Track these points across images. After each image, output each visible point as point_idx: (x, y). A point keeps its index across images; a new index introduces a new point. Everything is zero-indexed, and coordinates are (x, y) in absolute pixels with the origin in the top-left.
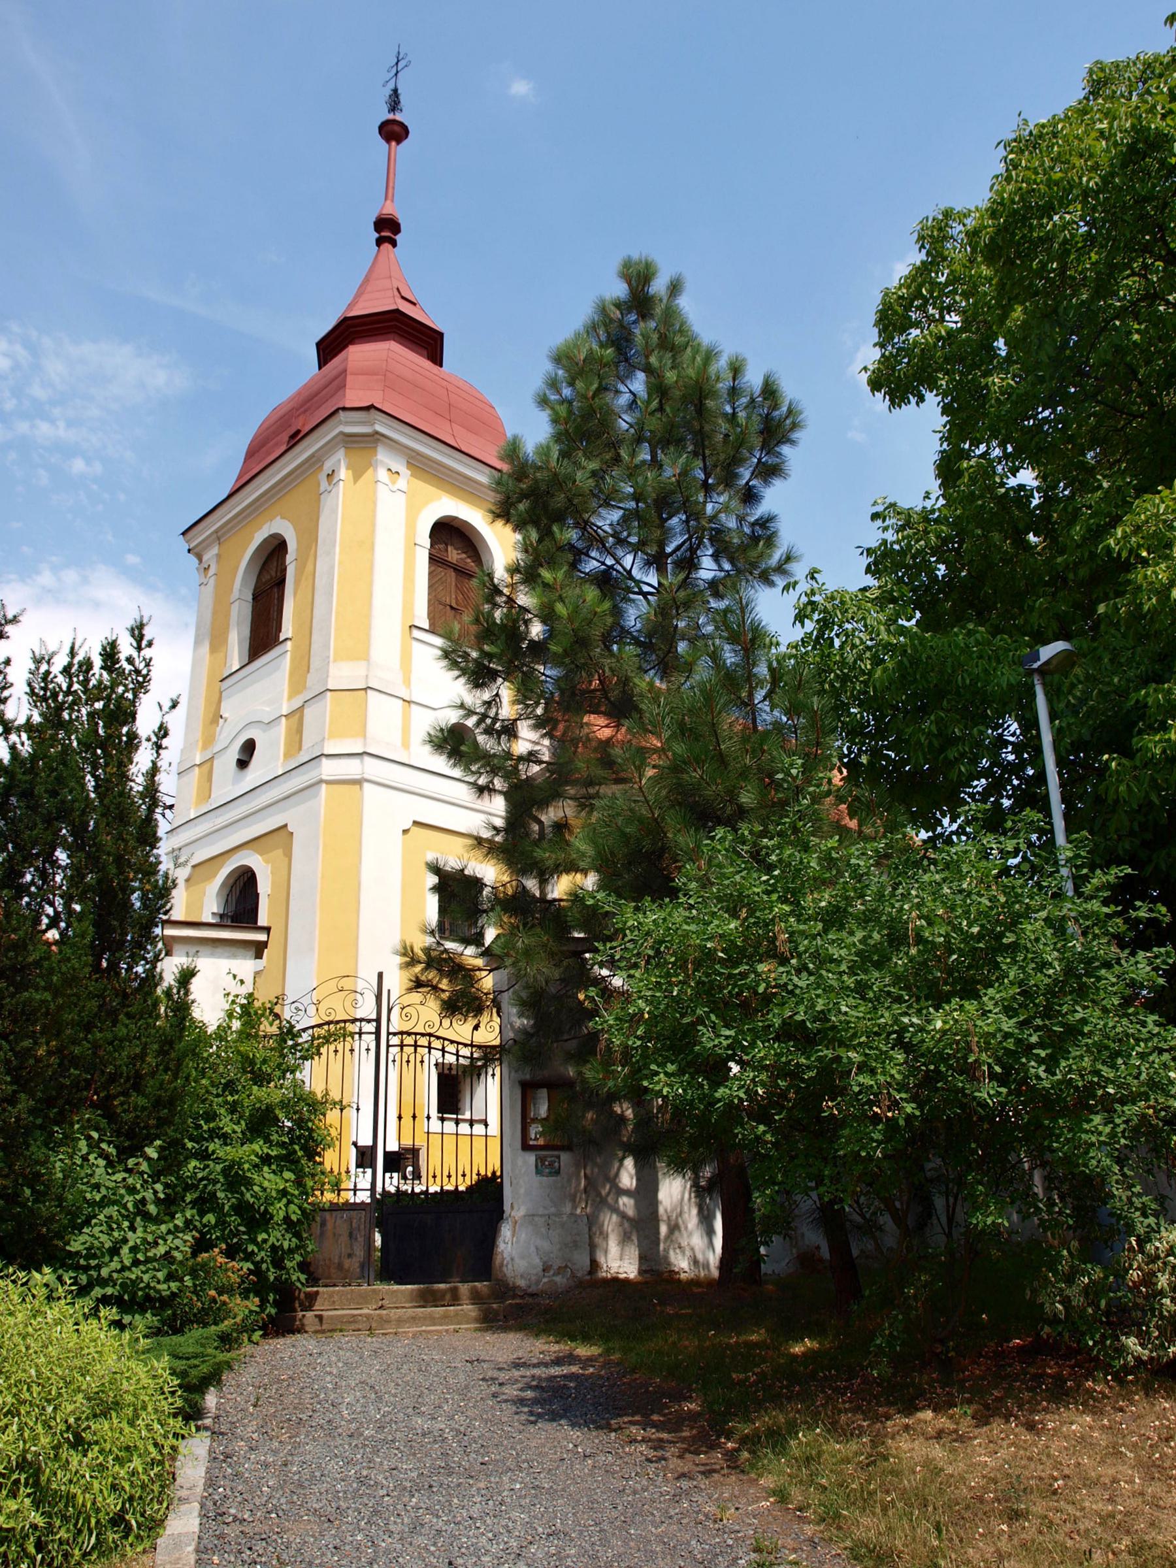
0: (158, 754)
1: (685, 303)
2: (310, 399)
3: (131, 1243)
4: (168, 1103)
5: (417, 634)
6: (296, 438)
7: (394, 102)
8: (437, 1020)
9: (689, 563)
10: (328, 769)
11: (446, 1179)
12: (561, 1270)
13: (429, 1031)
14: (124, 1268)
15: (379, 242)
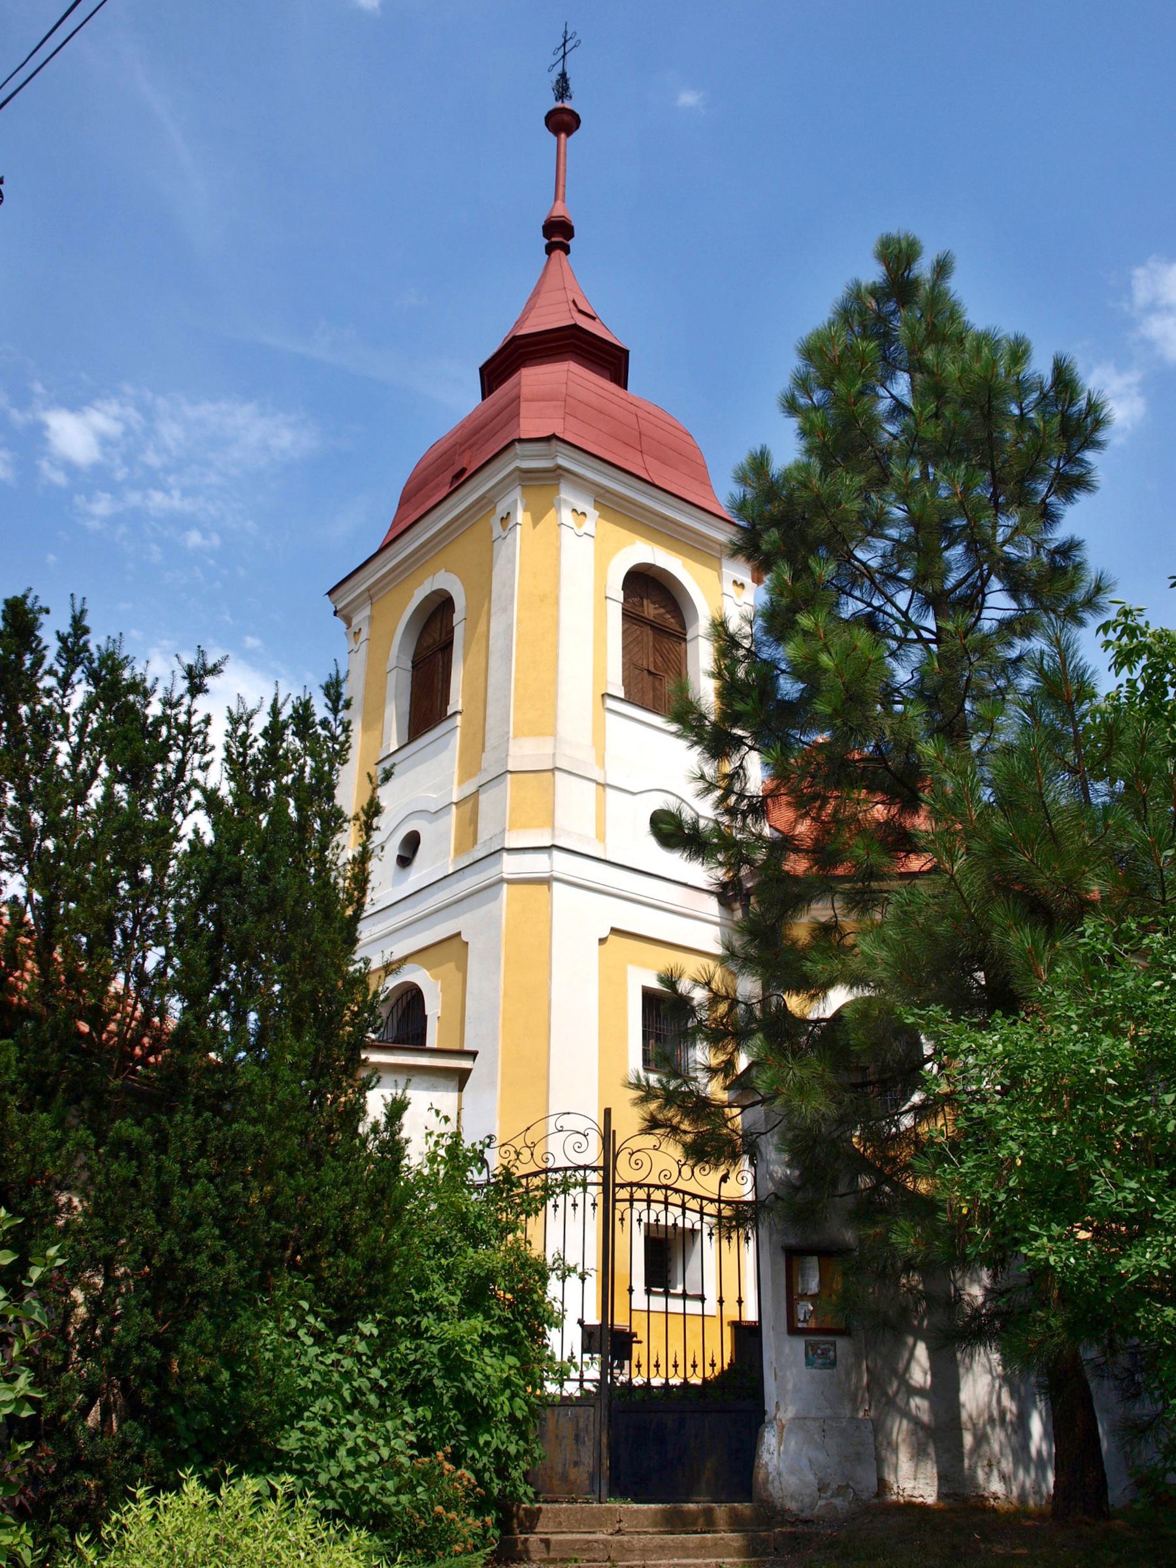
0: (369, 837)
1: (957, 286)
2: (476, 432)
3: (350, 1444)
4: (377, 1265)
5: (611, 704)
6: (461, 479)
7: (563, 88)
8: (674, 1169)
9: (974, 601)
10: (511, 865)
11: (690, 1370)
12: (840, 1491)
13: (664, 1182)
14: (343, 1475)
15: (549, 249)
